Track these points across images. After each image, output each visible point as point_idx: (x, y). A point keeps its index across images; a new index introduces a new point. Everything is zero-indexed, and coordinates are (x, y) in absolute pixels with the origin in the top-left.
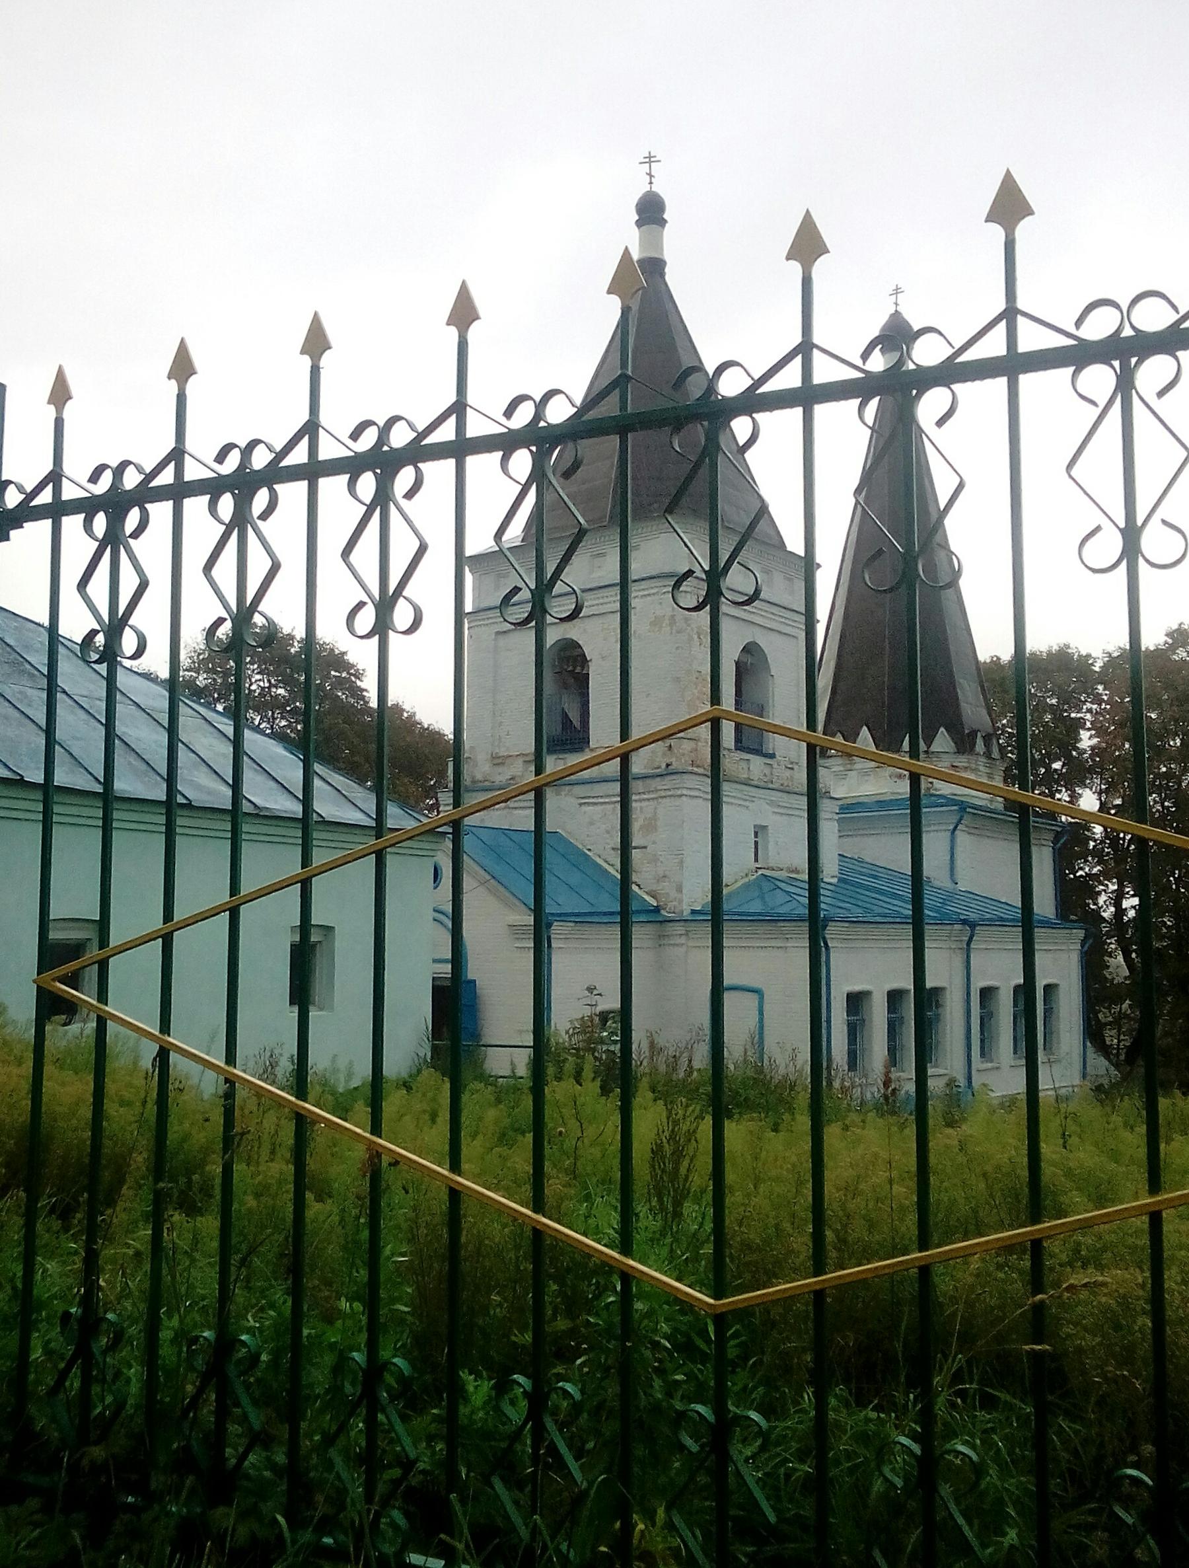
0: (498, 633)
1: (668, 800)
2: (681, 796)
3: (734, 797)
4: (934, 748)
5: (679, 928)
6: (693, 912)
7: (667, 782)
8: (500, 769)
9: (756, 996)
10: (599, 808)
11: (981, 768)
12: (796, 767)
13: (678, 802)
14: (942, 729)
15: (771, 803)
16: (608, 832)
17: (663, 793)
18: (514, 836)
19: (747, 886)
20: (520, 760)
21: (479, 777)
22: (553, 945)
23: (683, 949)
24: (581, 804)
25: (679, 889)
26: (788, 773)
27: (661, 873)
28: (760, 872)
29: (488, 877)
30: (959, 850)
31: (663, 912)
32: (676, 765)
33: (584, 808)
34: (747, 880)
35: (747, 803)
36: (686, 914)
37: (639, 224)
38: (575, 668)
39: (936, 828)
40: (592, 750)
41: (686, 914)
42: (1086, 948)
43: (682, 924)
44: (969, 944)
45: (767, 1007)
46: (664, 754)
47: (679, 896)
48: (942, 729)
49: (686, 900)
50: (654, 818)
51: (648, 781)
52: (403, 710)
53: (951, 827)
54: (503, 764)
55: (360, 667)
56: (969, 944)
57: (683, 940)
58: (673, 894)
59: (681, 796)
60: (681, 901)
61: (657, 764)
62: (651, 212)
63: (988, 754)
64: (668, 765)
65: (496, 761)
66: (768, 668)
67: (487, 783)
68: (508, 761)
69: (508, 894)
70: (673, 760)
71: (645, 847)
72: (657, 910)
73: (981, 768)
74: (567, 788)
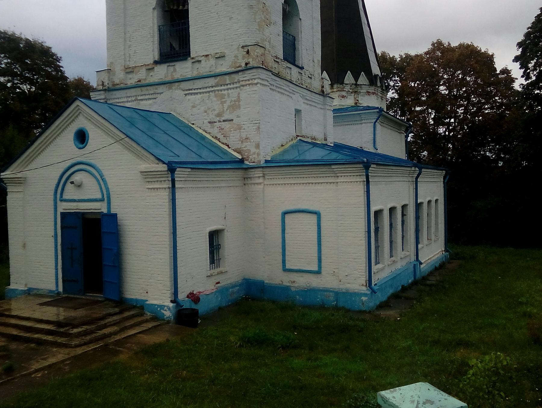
1: (248, 87)
2: (256, 84)
3: (285, 90)
4: (358, 83)
5: (258, 173)
6: (267, 161)
7: (248, 75)
8: (130, 76)
9: (314, 218)
10: (199, 96)
11: (379, 94)
12: (313, 77)
13: (255, 88)
14: (363, 73)
15: (303, 97)
16: (206, 112)
17: (244, 83)
18: (142, 113)
19: (292, 146)
20: (144, 69)
21: (117, 81)
22: (176, 186)
23: (261, 187)
24: (186, 95)
25: (258, 146)
26: (309, 80)
27: (244, 136)
28: (299, 138)
29: (123, 136)
30: (377, 132)
31: (246, 162)
32: (252, 63)
33: (189, 97)
34: (291, 143)
35: (291, 95)
36: (262, 163)
38: (178, 6)
39: (365, 121)
40: (193, 58)
41: (262, 163)
42: (446, 181)
43: (261, 169)
44: (417, 178)
45: (323, 224)
46: (244, 57)
47: (257, 151)
48: (363, 73)
49: (262, 154)
50: (239, 100)
51: (233, 76)
52: (84, 81)
53: (374, 121)
54: (133, 72)
55: (59, 55)
56: (417, 178)
57: (261, 180)
58: (253, 150)
59: (256, 84)
60: (258, 154)
61: (238, 65)
63: (381, 87)
64: (246, 64)
65: (128, 70)
66: (298, 14)
67: (122, 86)
68: (136, 70)
69: (139, 148)
70: (250, 60)
71: (232, 120)
72: (242, 161)
73: (379, 94)
74: (177, 84)
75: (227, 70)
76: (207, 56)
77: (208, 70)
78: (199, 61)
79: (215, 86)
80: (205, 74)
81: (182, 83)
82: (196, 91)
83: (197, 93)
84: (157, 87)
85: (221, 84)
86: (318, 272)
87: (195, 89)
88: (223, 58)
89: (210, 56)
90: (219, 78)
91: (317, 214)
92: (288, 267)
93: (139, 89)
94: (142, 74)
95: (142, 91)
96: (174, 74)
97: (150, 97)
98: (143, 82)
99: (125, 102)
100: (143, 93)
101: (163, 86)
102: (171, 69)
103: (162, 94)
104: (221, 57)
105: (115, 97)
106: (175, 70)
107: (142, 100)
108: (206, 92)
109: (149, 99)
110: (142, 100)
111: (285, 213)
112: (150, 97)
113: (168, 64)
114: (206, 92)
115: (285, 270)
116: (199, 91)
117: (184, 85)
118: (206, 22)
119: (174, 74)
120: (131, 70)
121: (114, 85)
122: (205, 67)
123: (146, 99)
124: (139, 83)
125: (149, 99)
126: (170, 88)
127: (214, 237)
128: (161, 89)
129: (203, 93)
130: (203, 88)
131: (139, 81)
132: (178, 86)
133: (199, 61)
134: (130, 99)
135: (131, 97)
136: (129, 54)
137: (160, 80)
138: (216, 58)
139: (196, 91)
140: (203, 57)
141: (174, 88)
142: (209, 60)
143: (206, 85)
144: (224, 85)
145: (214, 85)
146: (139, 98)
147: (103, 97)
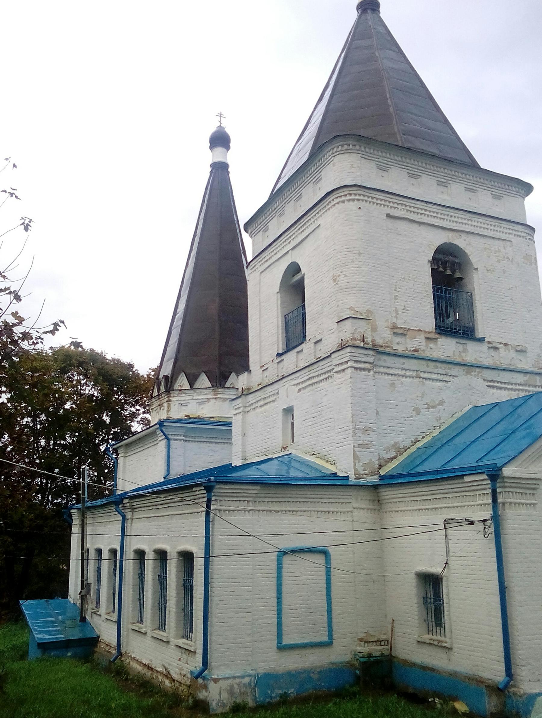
0: (388, 216)
9: (320, 559)
20: (423, 336)
21: (379, 341)
24: (488, 386)
37: (211, 148)
54: (405, 335)
62: (220, 140)
67: (388, 350)
74: (477, 370)
75: (530, 369)
76: (506, 345)
77: (508, 361)
78: (496, 349)
79: (522, 385)
80: (505, 366)
81: (484, 370)
82: (499, 385)
83: (500, 388)
84: (450, 366)
85: (530, 384)
86: (328, 644)
87: (498, 382)
88: (524, 353)
89: (510, 346)
90: (528, 376)
91: (325, 553)
92: (286, 641)
93: (424, 362)
94: (419, 342)
95: (428, 366)
96: (463, 355)
97: (439, 377)
98: (420, 354)
99: (399, 376)
100: (428, 370)
101: (459, 367)
102: (461, 347)
103: (456, 378)
104: (521, 351)
105: (384, 364)
106: (465, 351)
107: (426, 379)
108: (512, 389)
109: (437, 380)
110: (426, 379)
111: (285, 553)
112: (439, 377)
113: (457, 341)
114: (512, 389)
115: (282, 648)
116: (503, 386)
117: (488, 374)
118: (499, 304)
119: (463, 355)
120: (401, 331)
121: (374, 345)
122: (505, 358)
123: (433, 380)
124: (415, 353)
125: (437, 380)
126: (468, 373)
127: (431, 583)
128: (455, 371)
129: (508, 389)
130: (508, 384)
131: (416, 351)
132: (479, 373)
133: (496, 349)
134: (408, 373)
135: (410, 370)
136: (396, 308)
137: (447, 359)
138: (517, 351)
139: (499, 385)
140: (502, 345)
141: (473, 373)
142: (509, 351)
143: (514, 381)
144: (533, 386)
145: (523, 382)
146: (422, 375)
147: (371, 360)
